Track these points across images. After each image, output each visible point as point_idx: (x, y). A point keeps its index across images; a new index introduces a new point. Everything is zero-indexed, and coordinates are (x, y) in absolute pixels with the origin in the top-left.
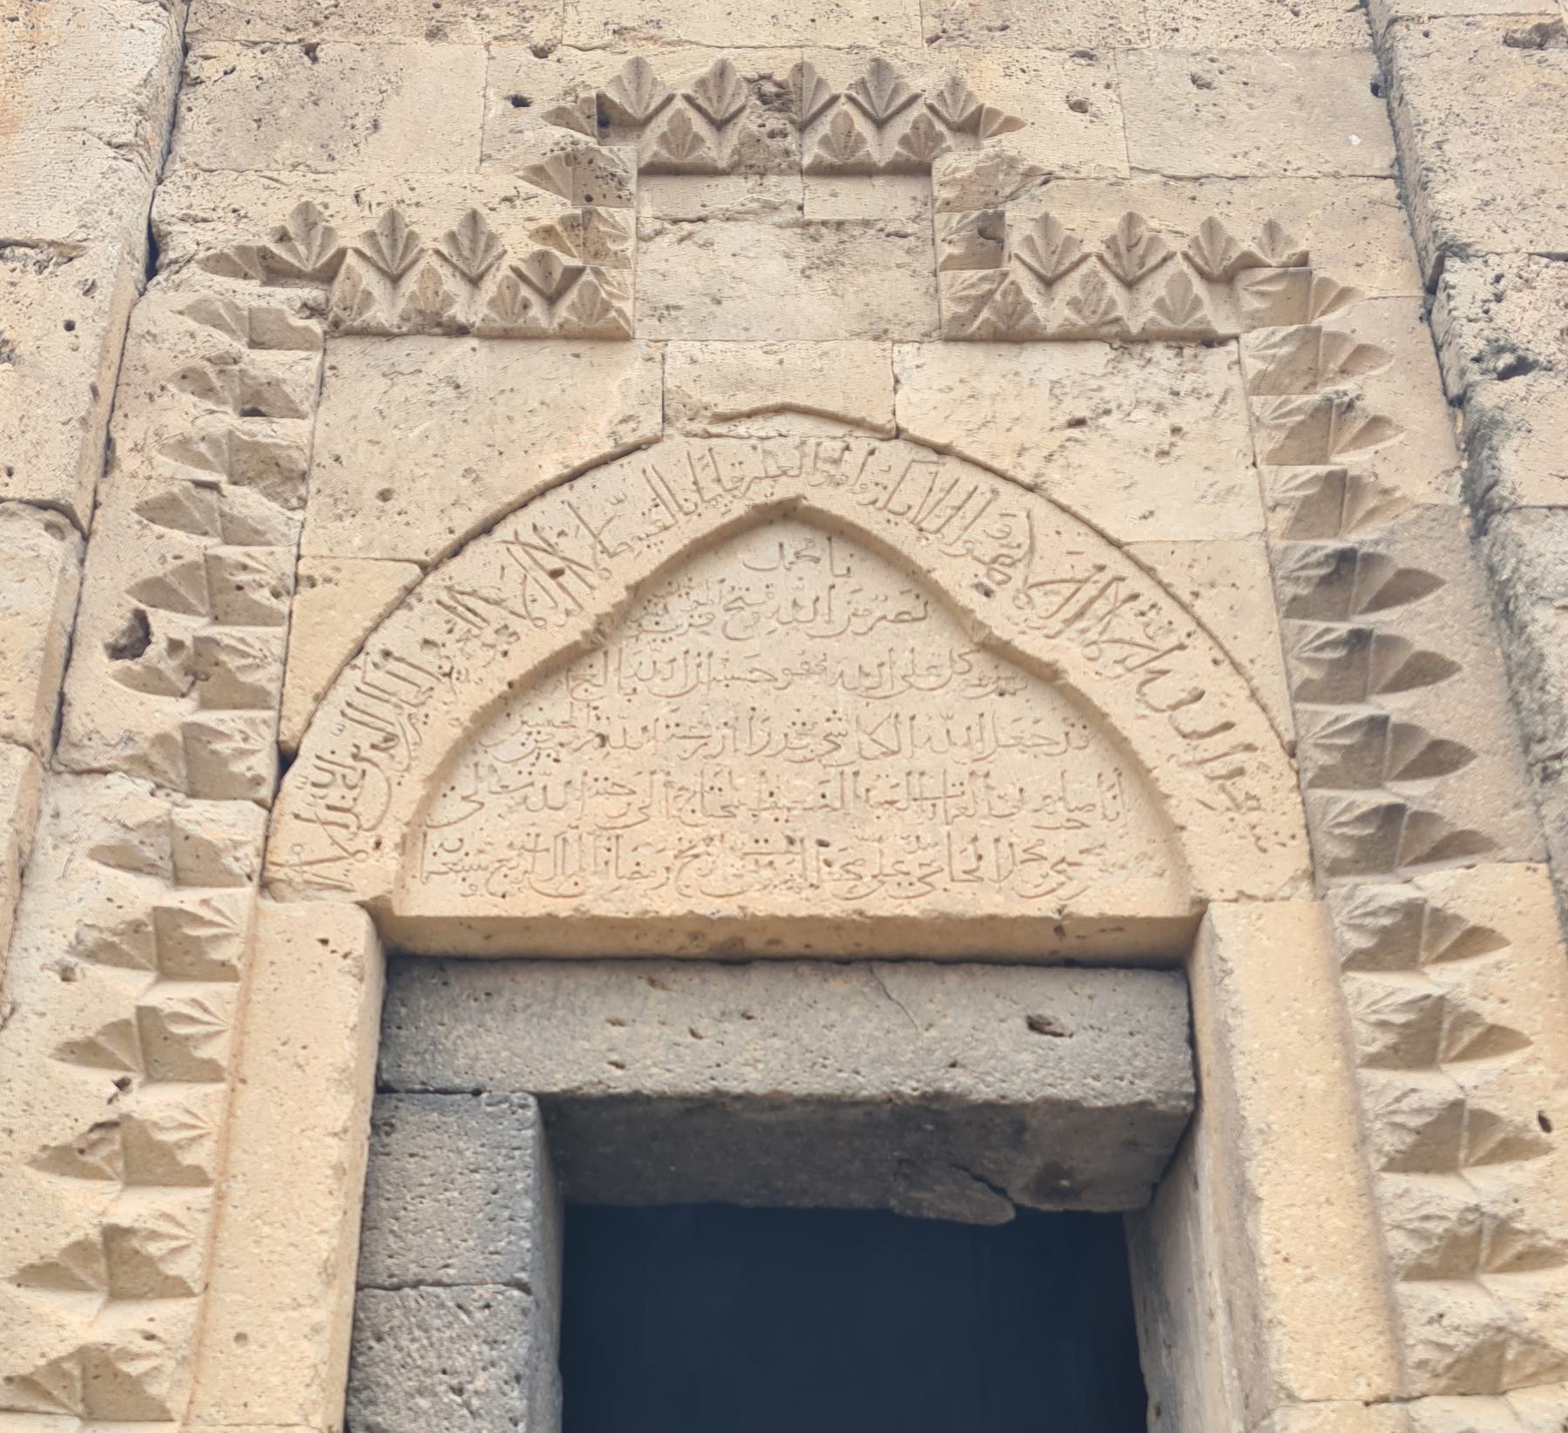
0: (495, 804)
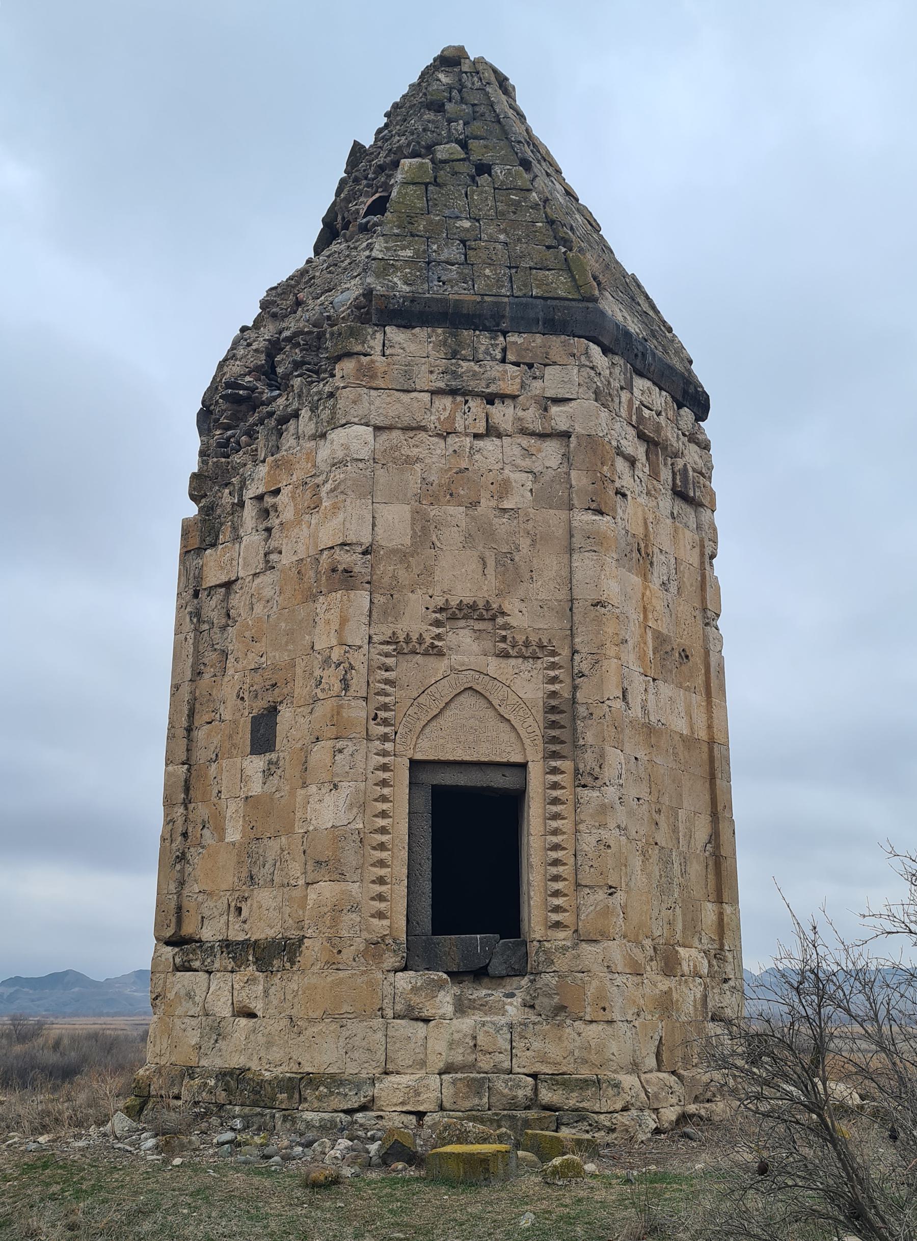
0: (426, 740)
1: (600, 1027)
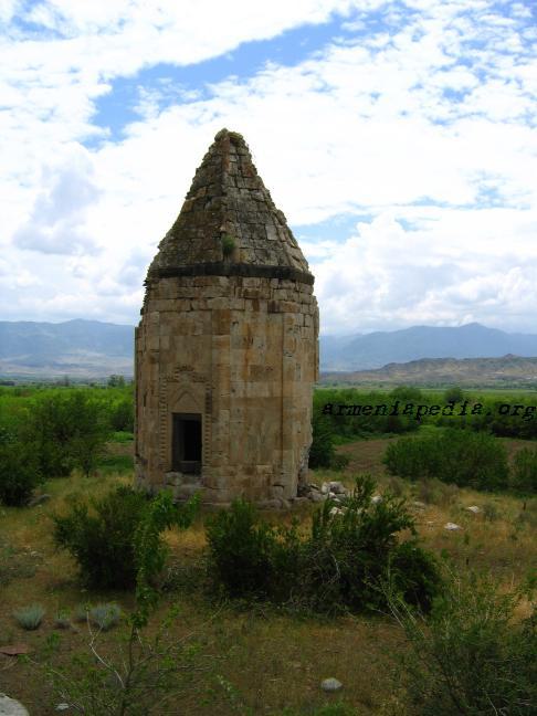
1: (60, 362)
